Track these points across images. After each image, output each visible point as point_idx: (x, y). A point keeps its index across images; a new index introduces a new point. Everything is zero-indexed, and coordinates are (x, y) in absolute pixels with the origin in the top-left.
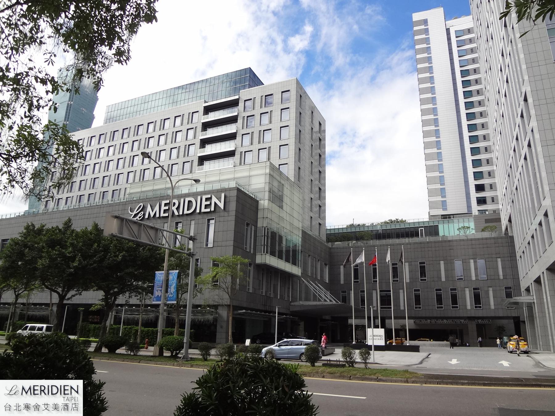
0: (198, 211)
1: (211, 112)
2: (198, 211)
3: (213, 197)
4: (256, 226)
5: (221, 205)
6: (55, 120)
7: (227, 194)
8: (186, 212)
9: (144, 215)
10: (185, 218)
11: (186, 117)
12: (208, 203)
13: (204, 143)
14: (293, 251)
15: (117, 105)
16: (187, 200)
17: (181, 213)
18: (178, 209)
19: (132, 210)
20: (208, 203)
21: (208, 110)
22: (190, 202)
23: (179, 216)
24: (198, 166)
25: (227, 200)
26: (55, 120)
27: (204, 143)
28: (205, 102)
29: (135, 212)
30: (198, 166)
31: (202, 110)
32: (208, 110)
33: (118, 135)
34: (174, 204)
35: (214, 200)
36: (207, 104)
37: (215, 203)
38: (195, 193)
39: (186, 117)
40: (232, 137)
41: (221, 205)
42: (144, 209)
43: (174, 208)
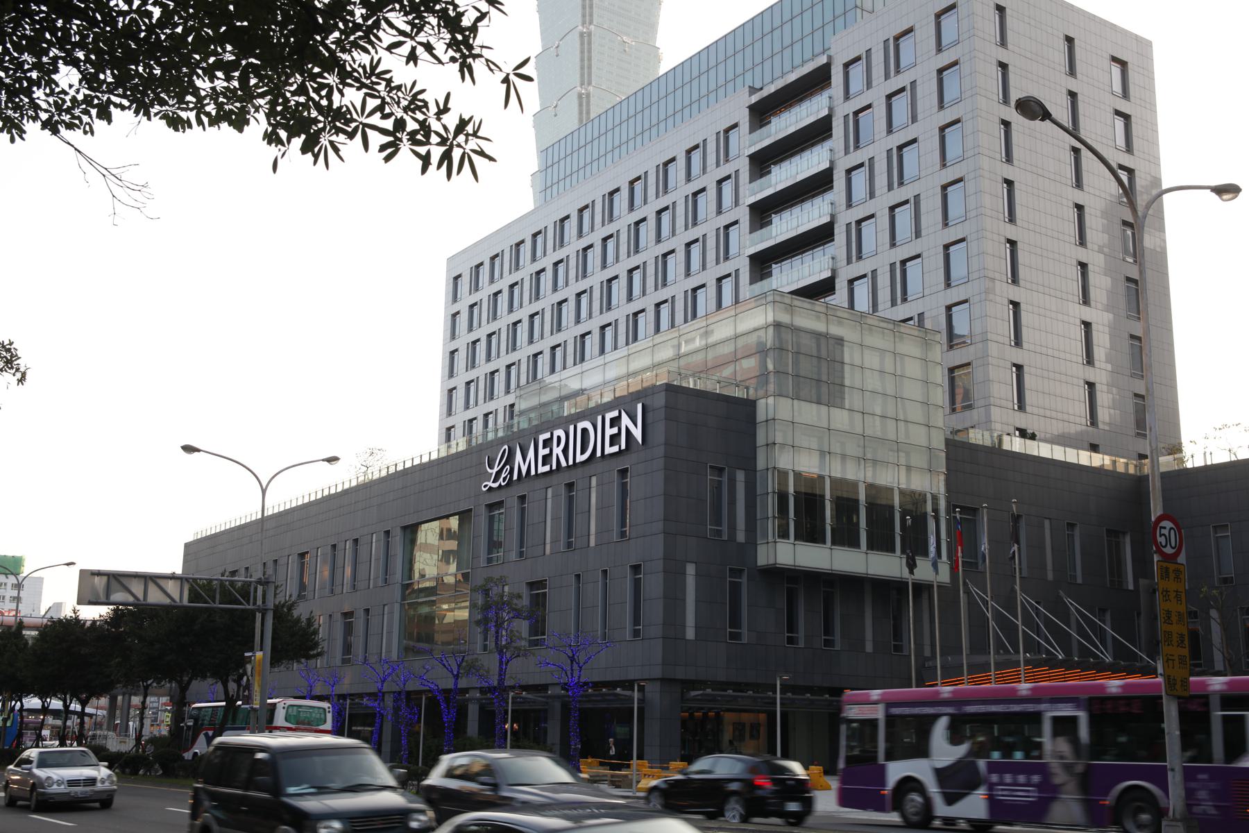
0: (599, 454)
1: (775, 114)
2: (599, 454)
3: (624, 415)
4: (751, 470)
5: (637, 433)
6: (11, 344)
7: (648, 402)
8: (580, 458)
9: (511, 472)
10: (579, 471)
11: (711, 147)
12: (615, 430)
13: (762, 212)
14: (871, 507)
15: (679, 71)
16: (581, 425)
17: (571, 462)
18: (565, 451)
19: (491, 467)
20: (615, 430)
21: (762, 112)
22: (585, 431)
23: (568, 466)
24: (751, 284)
25: (649, 420)
26: (11, 344)
27: (762, 212)
28: (753, 90)
29: (496, 469)
30: (751, 284)
31: (744, 117)
32: (762, 112)
33: (677, 172)
34: (559, 438)
35: (625, 421)
36: (755, 99)
37: (627, 429)
38: (638, 392)
39: (711, 147)
40: (819, 184)
41: (637, 433)
42: (510, 459)
43: (558, 451)
